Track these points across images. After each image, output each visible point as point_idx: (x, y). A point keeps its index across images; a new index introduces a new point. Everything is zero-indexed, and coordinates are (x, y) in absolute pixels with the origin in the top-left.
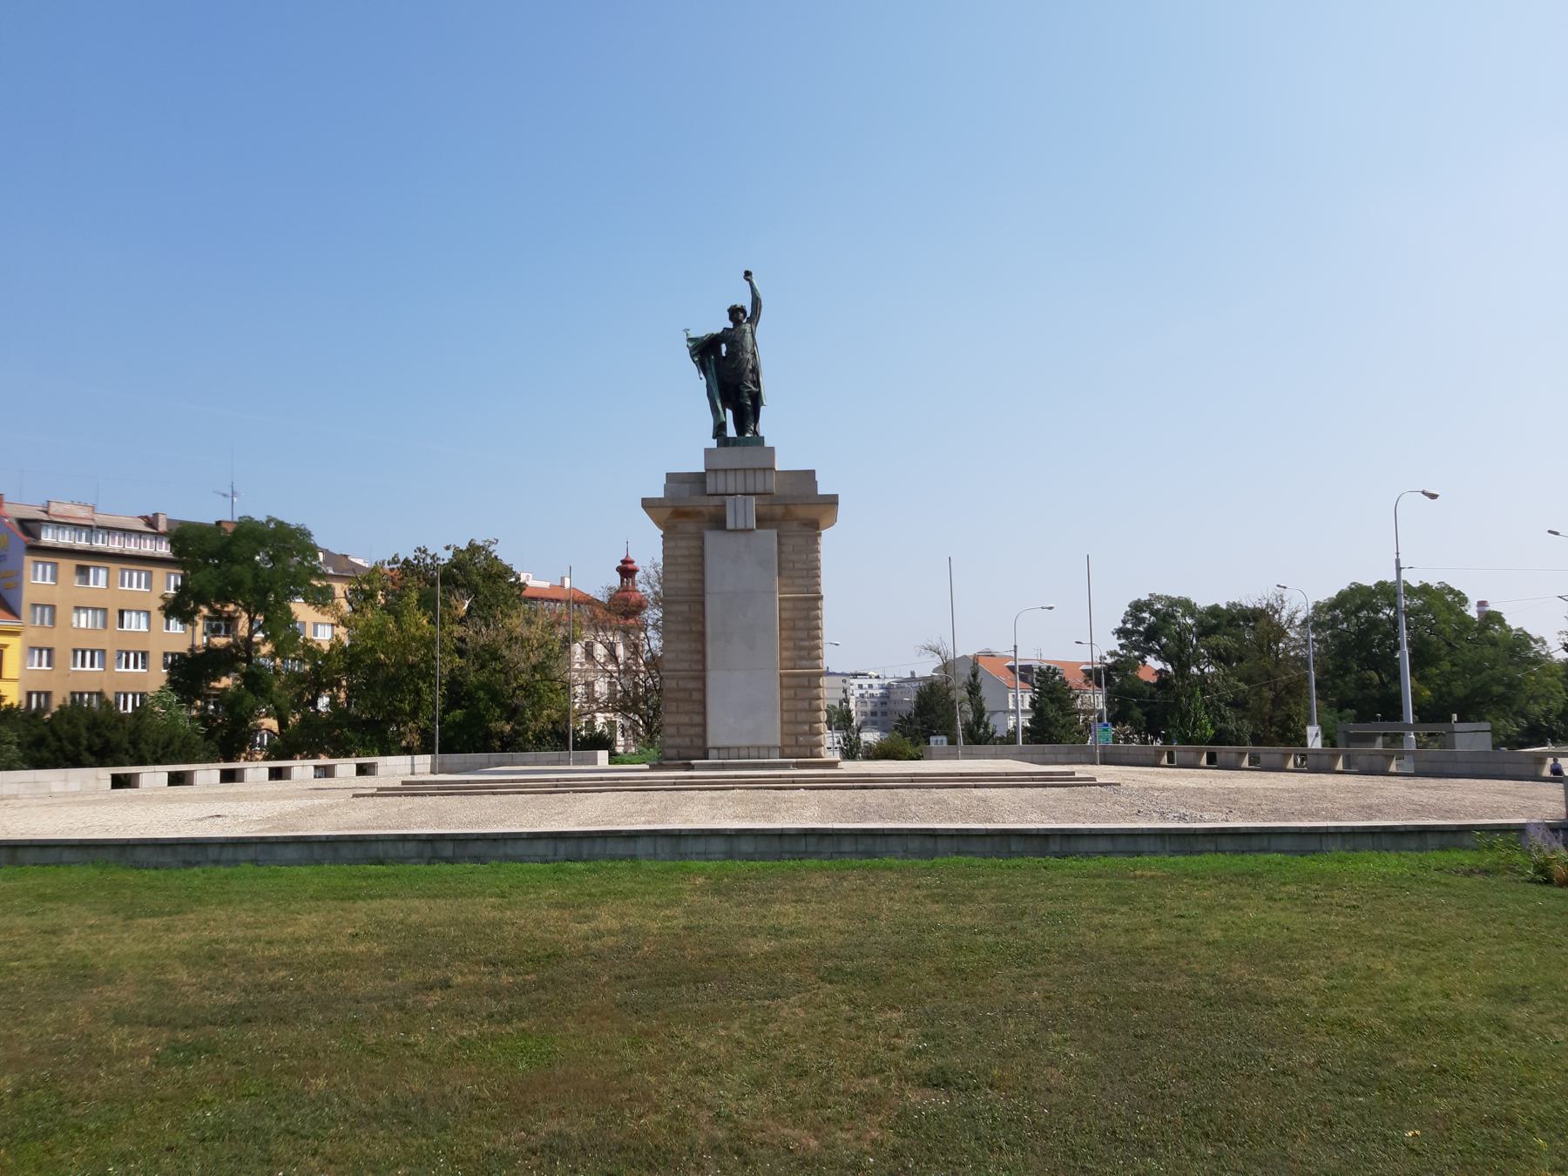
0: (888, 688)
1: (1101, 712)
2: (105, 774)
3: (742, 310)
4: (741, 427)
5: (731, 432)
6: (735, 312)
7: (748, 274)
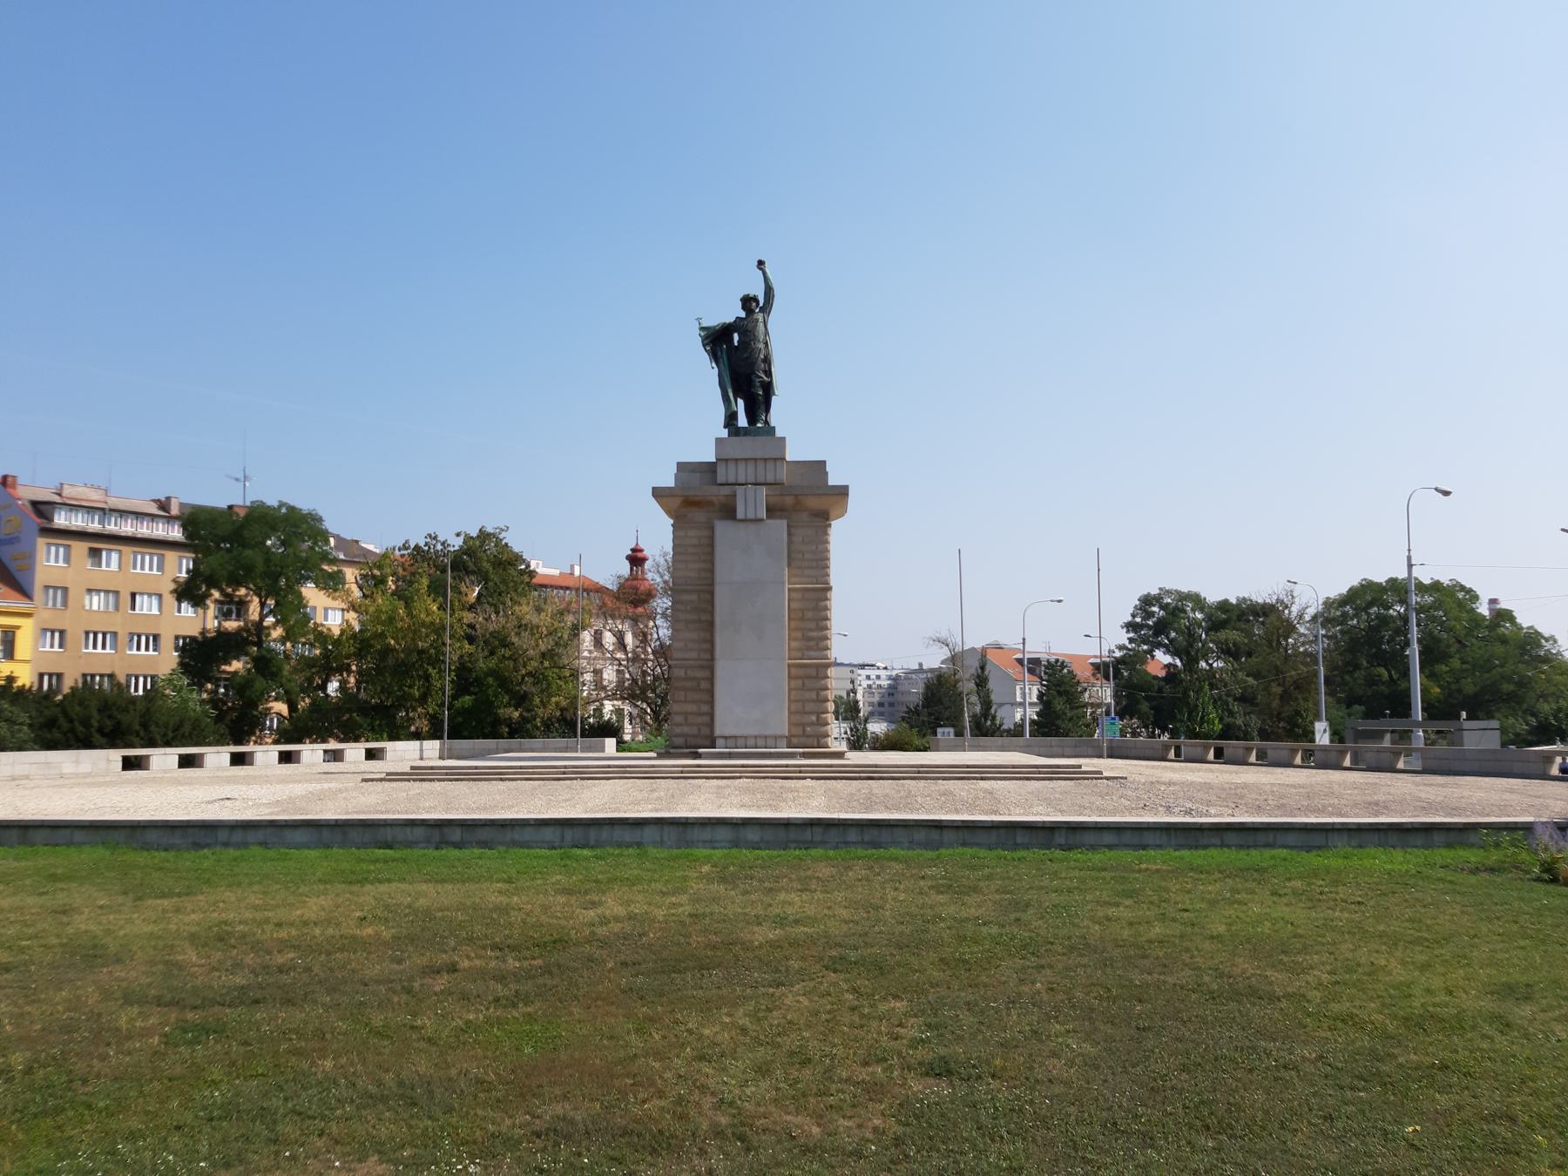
0: (896, 679)
1: (1109, 705)
2: (115, 756)
3: (755, 299)
4: (752, 418)
5: (742, 421)
6: (748, 302)
7: (761, 263)
